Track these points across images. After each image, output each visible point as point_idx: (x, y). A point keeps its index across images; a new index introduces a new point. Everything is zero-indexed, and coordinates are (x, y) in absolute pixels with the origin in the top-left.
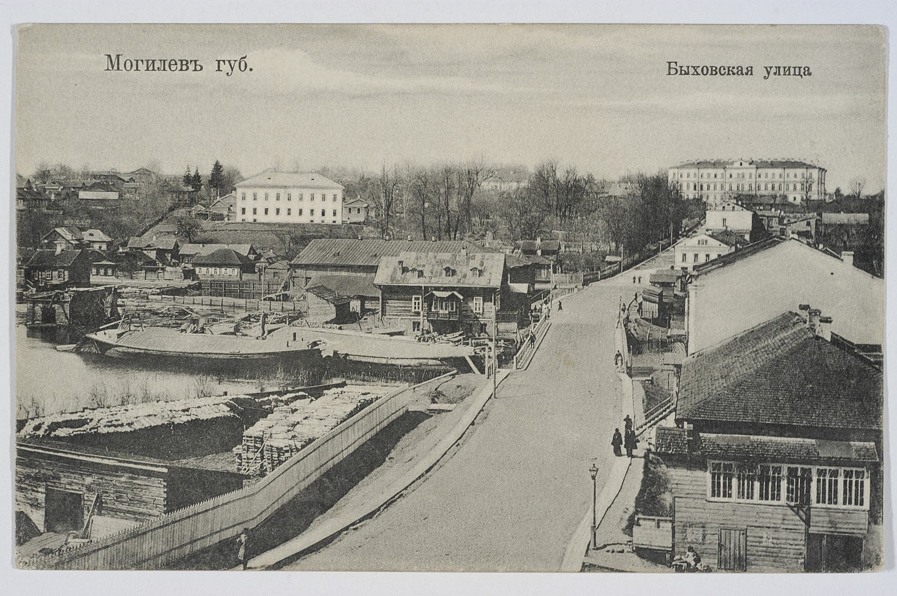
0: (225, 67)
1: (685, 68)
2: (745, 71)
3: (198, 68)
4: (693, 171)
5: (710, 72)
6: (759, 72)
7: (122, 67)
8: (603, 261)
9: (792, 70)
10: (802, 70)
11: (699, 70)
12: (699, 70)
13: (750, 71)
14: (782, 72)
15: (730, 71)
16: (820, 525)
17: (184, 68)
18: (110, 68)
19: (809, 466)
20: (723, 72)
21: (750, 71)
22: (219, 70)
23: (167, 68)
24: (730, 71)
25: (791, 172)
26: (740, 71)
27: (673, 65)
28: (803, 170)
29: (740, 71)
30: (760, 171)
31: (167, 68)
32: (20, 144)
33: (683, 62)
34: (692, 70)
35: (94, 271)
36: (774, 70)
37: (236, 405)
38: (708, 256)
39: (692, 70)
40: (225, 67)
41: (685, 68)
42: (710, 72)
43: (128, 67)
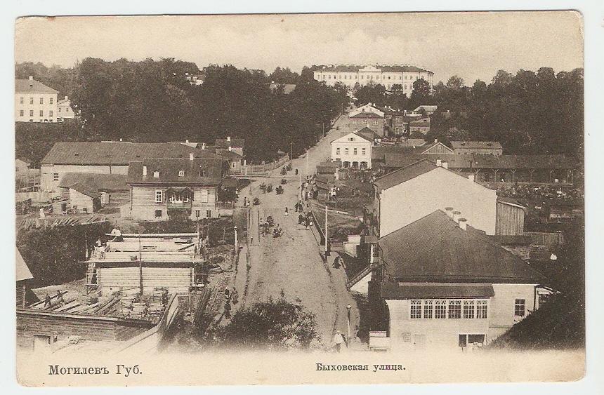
0: (123, 371)
2: (363, 368)
3: (106, 372)
5: (87, 370)
6: (371, 368)
7: (59, 372)
8: (100, 190)
9: (391, 367)
11: (336, 368)
12: (336, 368)
13: (366, 368)
15: (355, 368)
19: (489, 284)
21: (366, 368)
22: (118, 373)
24: (355, 368)
25: (408, 74)
26: (360, 368)
28: (417, 74)
29: (360, 368)
30: (383, 74)
31: (87, 372)
32: (18, 48)
39: (331, 368)
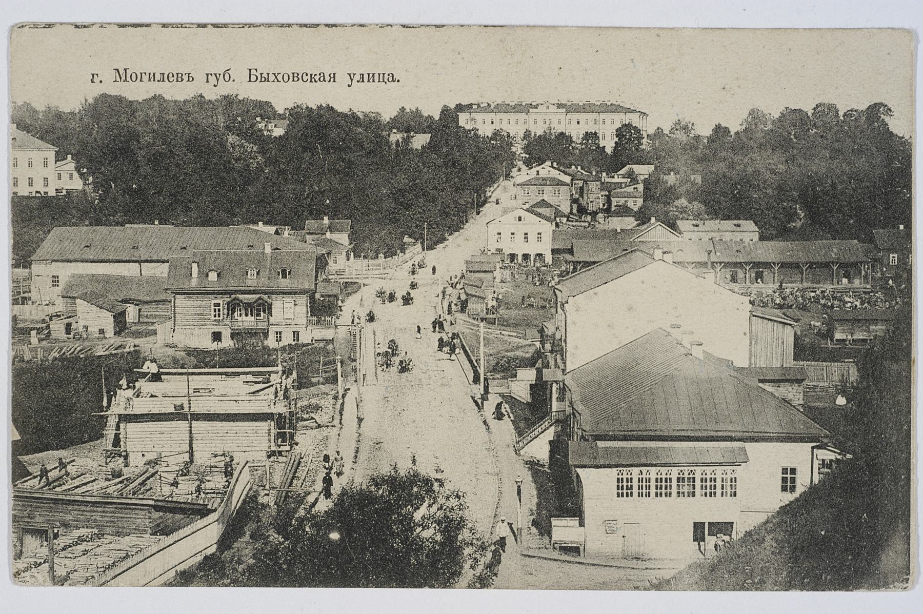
0: (212, 79)
1: (265, 75)
3: (191, 79)
4: (730, 233)
5: (300, 76)
10: (386, 76)
14: (366, 79)
16: (28, 270)
17: (180, 79)
18: (118, 79)
20: (305, 78)
23: (166, 79)
27: (253, 72)
33: (263, 68)
34: (272, 78)
35: (123, 382)
36: (357, 77)
37: (230, 547)
38: (277, 233)
39: (272, 78)
40: (212, 79)
41: (265, 75)
42: (300, 76)
43: (134, 79)
